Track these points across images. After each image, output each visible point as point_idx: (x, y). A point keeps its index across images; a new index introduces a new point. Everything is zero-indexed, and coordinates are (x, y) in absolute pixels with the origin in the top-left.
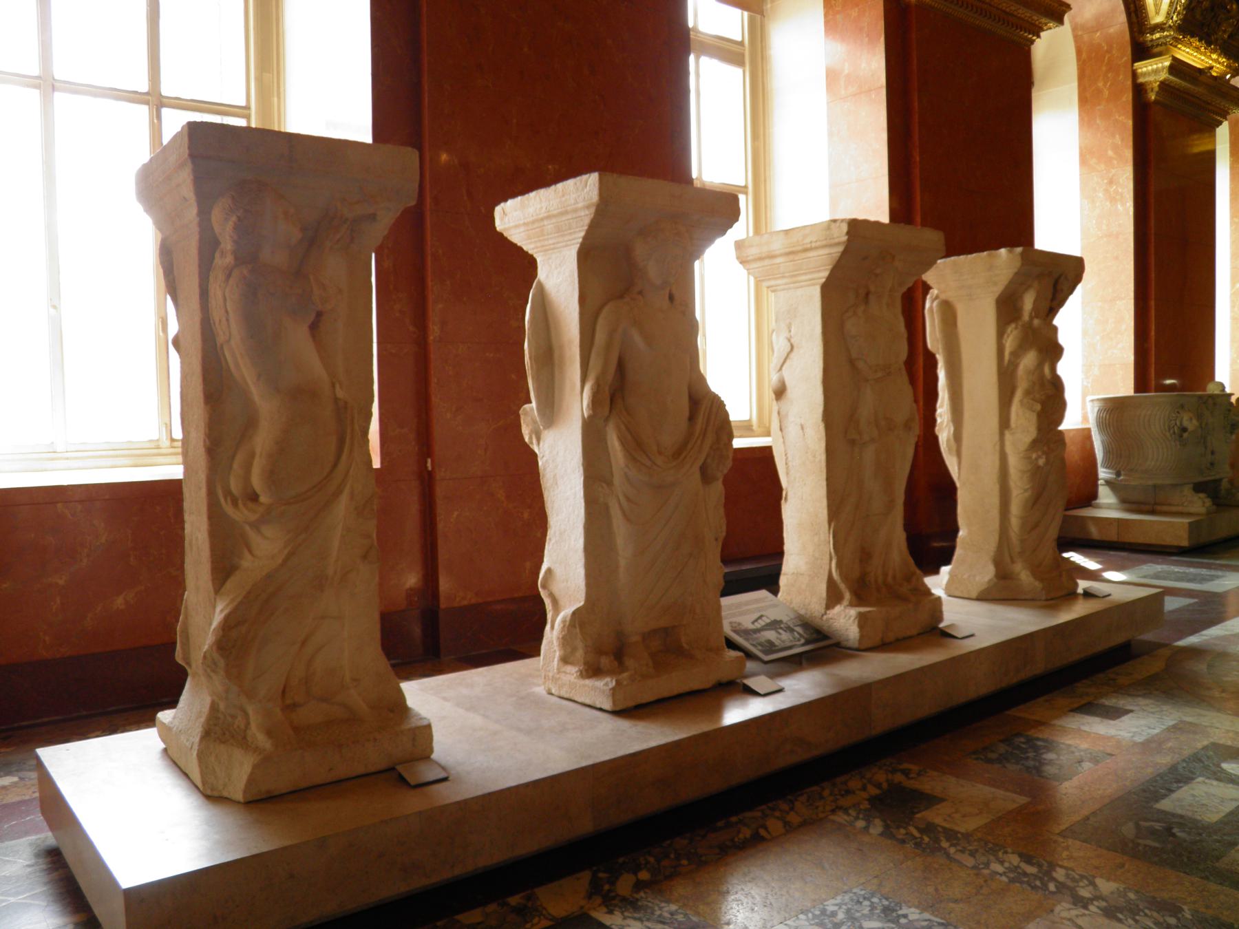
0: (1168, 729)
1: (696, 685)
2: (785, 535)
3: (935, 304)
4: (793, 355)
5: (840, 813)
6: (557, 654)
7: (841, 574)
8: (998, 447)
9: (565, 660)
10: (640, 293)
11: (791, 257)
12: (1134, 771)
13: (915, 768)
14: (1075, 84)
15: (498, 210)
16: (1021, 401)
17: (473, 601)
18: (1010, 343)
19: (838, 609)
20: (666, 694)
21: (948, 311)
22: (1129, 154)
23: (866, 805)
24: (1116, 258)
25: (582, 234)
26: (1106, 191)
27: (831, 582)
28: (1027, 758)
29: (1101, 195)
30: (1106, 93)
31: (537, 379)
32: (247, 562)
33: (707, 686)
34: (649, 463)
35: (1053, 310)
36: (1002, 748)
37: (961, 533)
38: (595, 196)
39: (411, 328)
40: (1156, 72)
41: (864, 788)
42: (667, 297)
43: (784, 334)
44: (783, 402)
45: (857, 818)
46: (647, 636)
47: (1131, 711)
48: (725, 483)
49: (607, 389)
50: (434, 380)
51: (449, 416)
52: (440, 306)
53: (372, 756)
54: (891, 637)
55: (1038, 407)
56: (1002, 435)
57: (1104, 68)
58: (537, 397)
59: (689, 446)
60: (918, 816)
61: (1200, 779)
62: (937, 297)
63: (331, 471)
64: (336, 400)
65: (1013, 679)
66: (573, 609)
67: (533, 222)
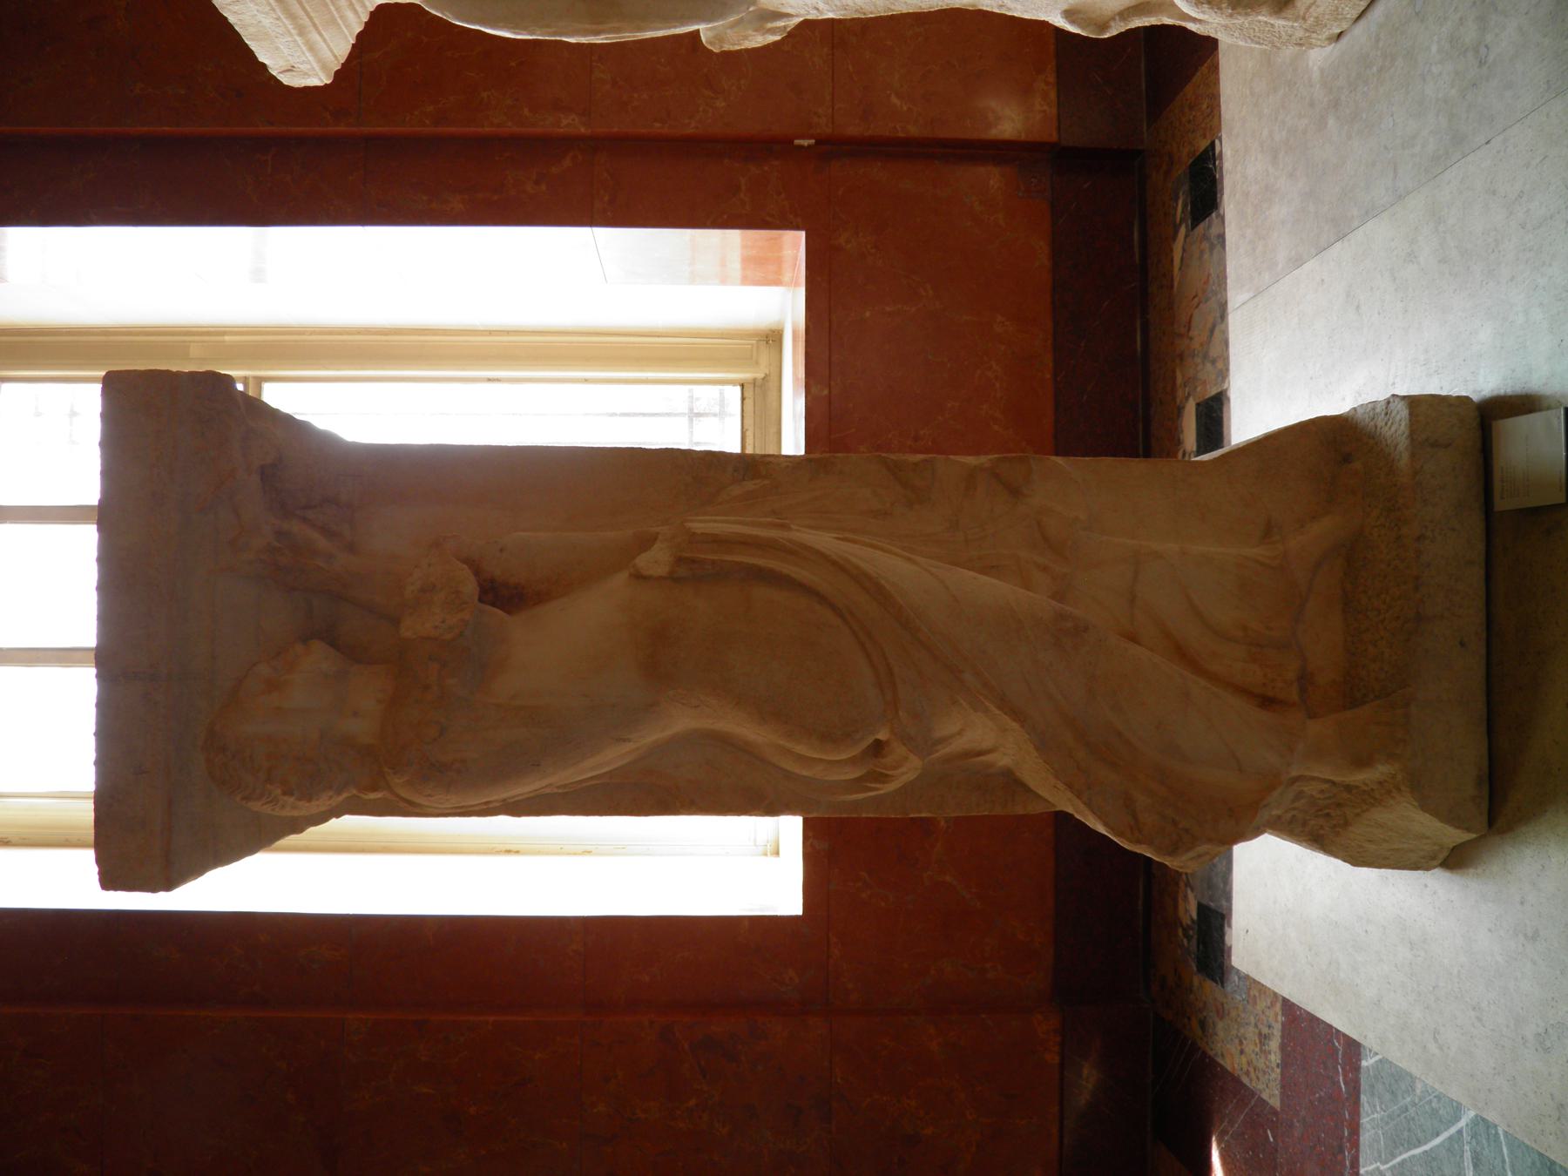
17: (1052, 79)
31: (644, 20)
32: (1002, 760)
39: (567, 162)
50: (658, 128)
51: (720, 104)
52: (526, 111)
53: (1450, 546)
63: (833, 607)
64: (673, 578)
67: (292, 17)
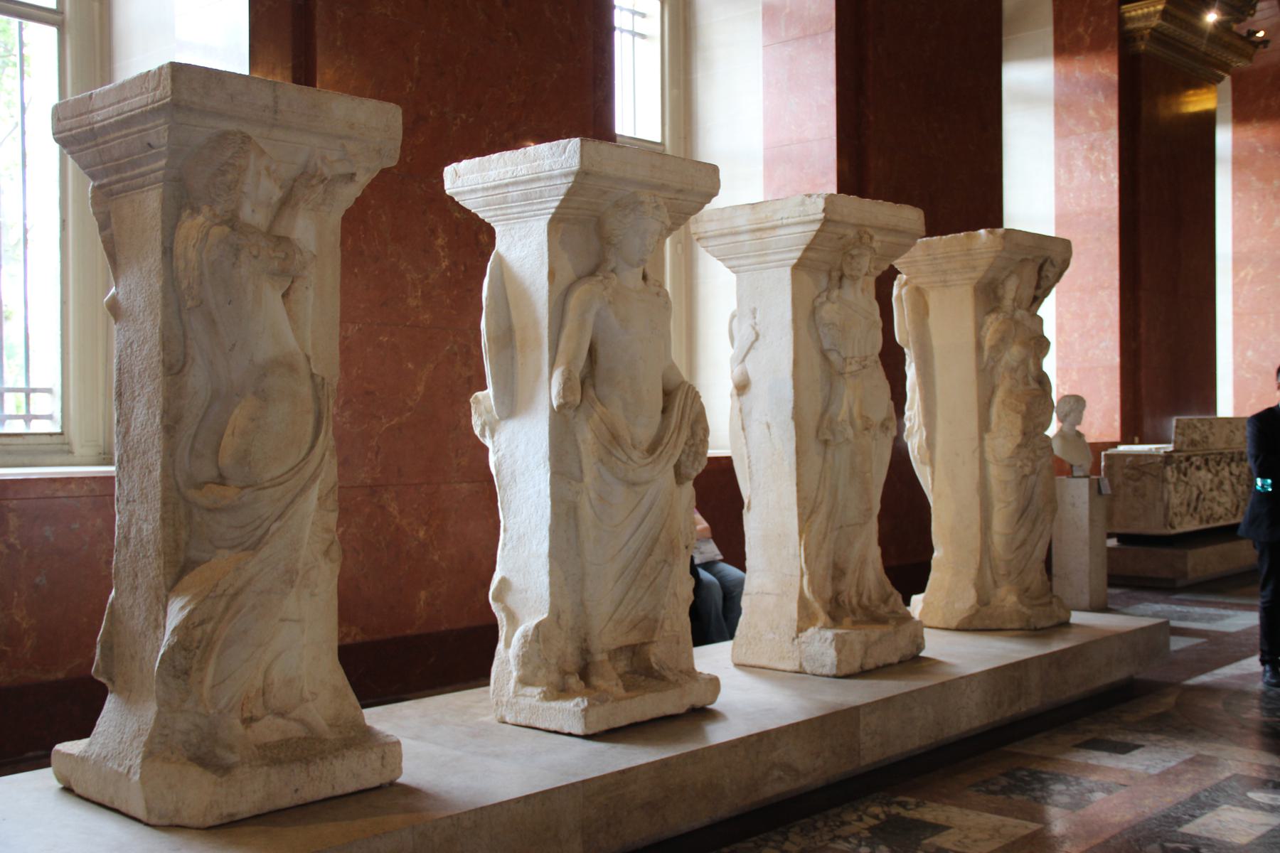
0: (1185, 762)
1: (669, 709)
2: (747, 549)
3: (904, 291)
4: (757, 344)
5: (840, 841)
6: (515, 674)
7: (814, 592)
8: (977, 455)
9: (524, 681)
10: (613, 271)
11: (758, 234)
12: (1154, 803)
13: (911, 800)
14: (1050, 29)
15: (449, 171)
16: (1003, 402)
17: (359, 638)
18: (989, 338)
19: (811, 630)
20: (638, 718)
21: (919, 294)
22: (1113, 114)
23: (866, 834)
24: (1098, 239)
25: (556, 204)
26: (1086, 158)
27: (803, 603)
28: (1033, 790)
29: (1080, 163)
30: (1088, 40)
33: (682, 710)
34: (624, 458)
35: (1037, 300)
36: (1004, 781)
37: (935, 554)
38: (575, 164)
40: (1147, 17)
41: (860, 819)
42: (640, 276)
43: (748, 322)
44: (744, 398)
45: (860, 845)
46: (614, 654)
47: (1142, 746)
48: (695, 485)
49: (578, 376)
54: (870, 664)
55: (1024, 408)
56: (981, 439)
57: (1085, 10)
58: (495, 384)
59: (665, 440)
60: (926, 842)
61: (1225, 806)
62: (906, 284)
65: (1007, 712)
66: (535, 622)
